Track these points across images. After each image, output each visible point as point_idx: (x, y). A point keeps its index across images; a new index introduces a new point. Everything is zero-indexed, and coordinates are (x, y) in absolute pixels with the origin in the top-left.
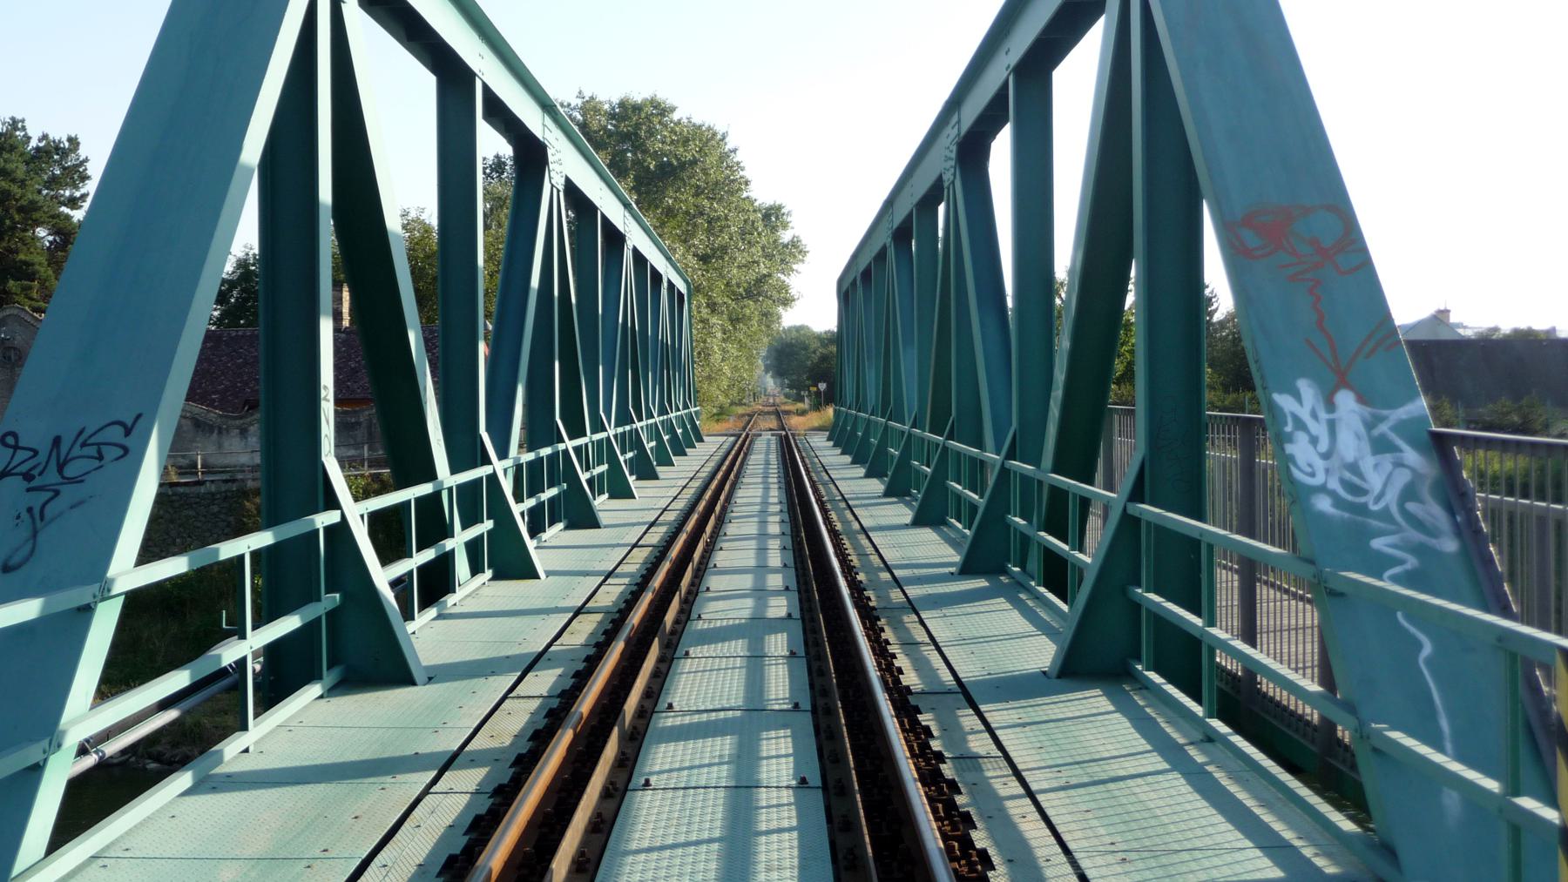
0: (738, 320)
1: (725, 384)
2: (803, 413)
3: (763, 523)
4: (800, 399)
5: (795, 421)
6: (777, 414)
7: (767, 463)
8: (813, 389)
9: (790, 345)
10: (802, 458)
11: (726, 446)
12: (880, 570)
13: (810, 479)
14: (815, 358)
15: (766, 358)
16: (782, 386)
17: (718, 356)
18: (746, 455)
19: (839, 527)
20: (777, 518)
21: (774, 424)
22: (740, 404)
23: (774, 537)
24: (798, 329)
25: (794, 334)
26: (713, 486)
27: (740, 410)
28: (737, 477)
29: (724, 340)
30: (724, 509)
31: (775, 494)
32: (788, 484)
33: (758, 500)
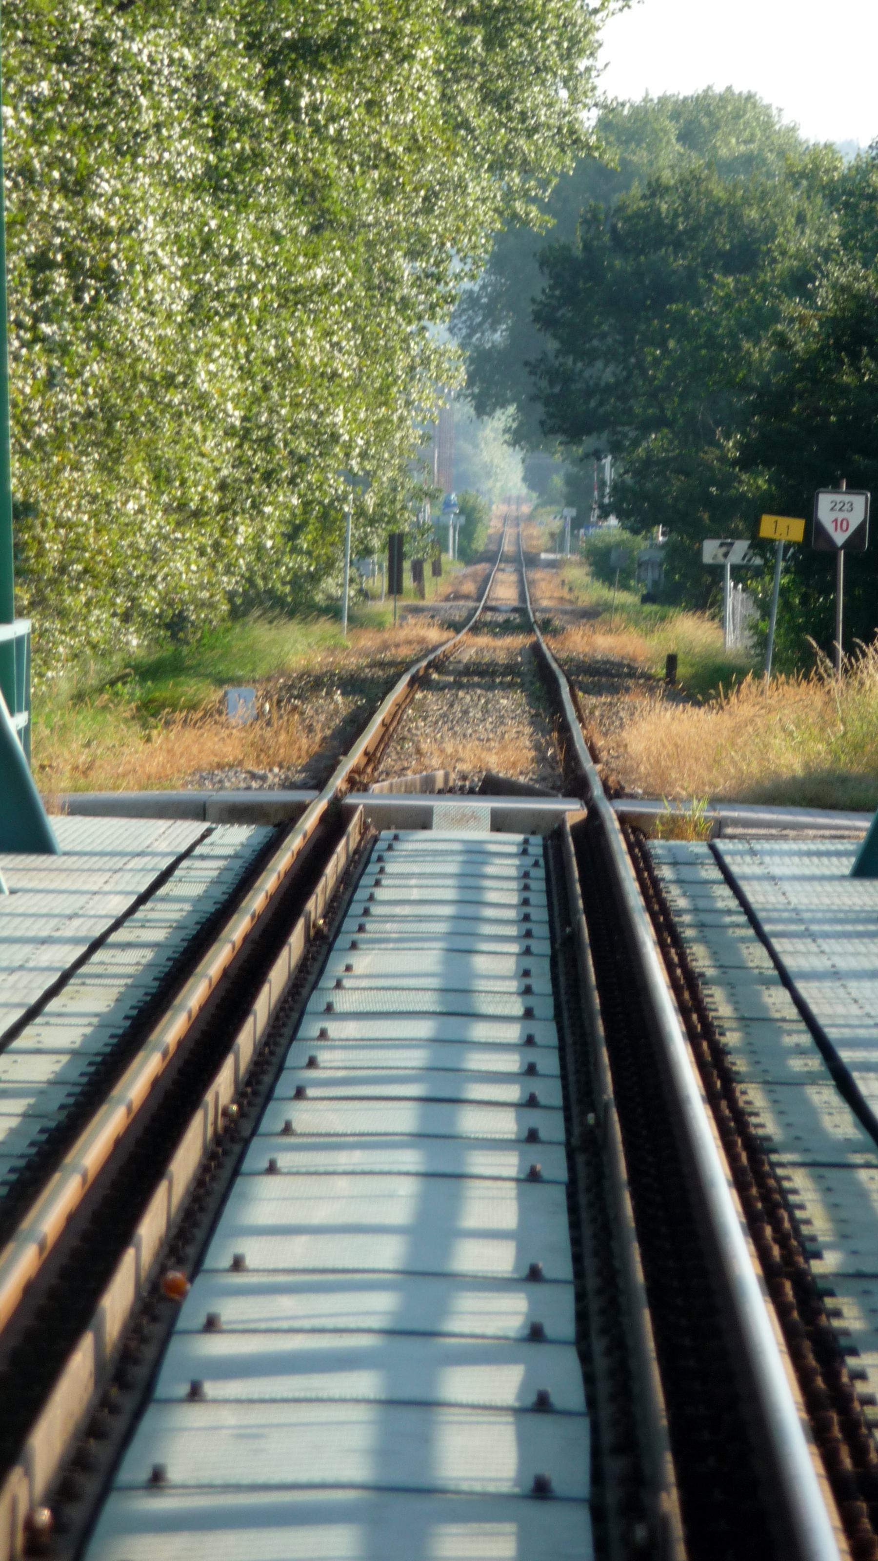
0: (309, 52)
1: (211, 457)
2: (704, 684)
3: (410, 1411)
4: (690, 587)
5: (649, 737)
6: (543, 686)
7: (457, 1006)
8: (786, 530)
9: (644, 234)
10: (687, 985)
11: (194, 885)
12: (767, 982)
13: (734, 1126)
14: (802, 323)
15: (477, 310)
16: (578, 494)
17: (170, 292)
18: (321, 946)
19: (767, 1124)
20: (504, 1384)
21: (505, 741)
22: (296, 603)
23: (480, 1507)
24: (699, 119)
25: (669, 159)
26: (218, 960)
27: (300, 647)
28: (257, 1089)
29: (213, 183)
30: (158, 1306)
31: (499, 1218)
32: (585, 1150)
33: (387, 1254)
